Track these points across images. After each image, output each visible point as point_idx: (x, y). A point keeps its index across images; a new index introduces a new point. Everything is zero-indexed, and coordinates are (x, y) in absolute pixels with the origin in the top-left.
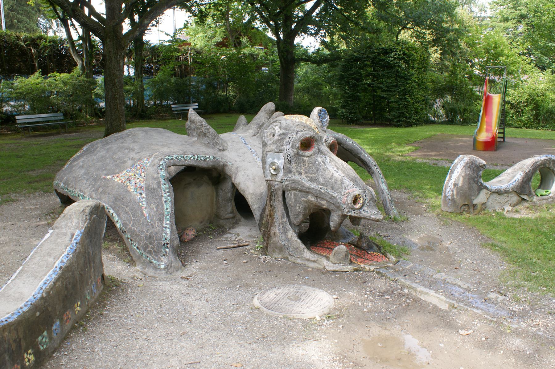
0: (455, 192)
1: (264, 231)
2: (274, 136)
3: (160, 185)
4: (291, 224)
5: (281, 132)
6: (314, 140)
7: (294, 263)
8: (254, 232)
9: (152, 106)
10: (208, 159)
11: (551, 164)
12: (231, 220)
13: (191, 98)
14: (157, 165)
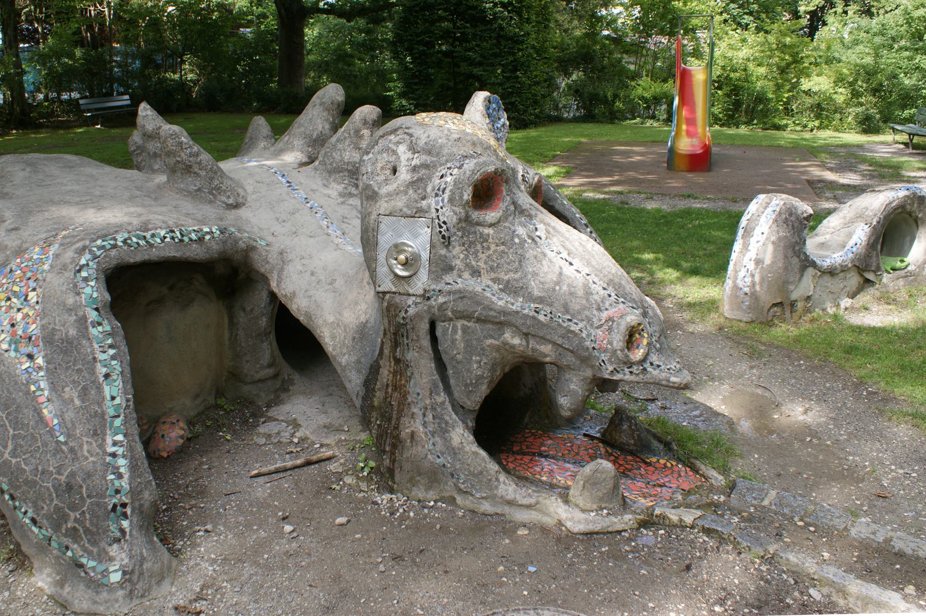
0: (757, 279)
1: (379, 426)
2: (394, 171)
3: (87, 328)
5: (416, 162)
7: (473, 512)
8: (335, 413)
9: (40, 104)
10: (208, 237)
11: (916, 205)
12: (270, 383)
13: (115, 85)
14: (71, 267)
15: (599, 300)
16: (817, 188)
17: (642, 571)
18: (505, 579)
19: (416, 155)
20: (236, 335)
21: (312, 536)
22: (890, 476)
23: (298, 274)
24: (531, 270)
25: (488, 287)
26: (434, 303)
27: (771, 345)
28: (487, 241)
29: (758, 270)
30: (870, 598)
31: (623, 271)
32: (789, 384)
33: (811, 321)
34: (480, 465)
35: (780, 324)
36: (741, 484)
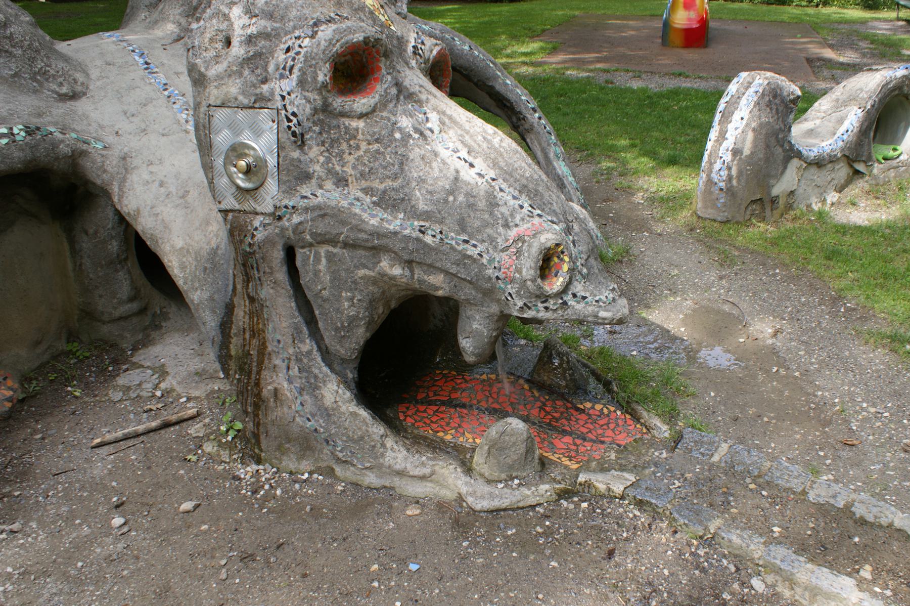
0: (734, 172)
2: (228, 43)
4: (326, 354)
5: (253, 30)
6: (378, 52)
7: (356, 485)
12: (135, 320)
15: (507, 213)
16: (816, 64)
17: (553, 563)
18: (376, 584)
19: (254, 20)
20: (81, 265)
21: (147, 529)
22: (860, 417)
23: (144, 185)
24: (415, 175)
25: (358, 199)
26: (287, 224)
27: (746, 250)
28: (355, 137)
29: (735, 162)
30: (819, 589)
31: (541, 173)
32: (760, 298)
33: (793, 219)
34: (359, 429)
35: (759, 224)
36: (690, 436)
